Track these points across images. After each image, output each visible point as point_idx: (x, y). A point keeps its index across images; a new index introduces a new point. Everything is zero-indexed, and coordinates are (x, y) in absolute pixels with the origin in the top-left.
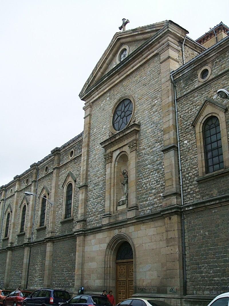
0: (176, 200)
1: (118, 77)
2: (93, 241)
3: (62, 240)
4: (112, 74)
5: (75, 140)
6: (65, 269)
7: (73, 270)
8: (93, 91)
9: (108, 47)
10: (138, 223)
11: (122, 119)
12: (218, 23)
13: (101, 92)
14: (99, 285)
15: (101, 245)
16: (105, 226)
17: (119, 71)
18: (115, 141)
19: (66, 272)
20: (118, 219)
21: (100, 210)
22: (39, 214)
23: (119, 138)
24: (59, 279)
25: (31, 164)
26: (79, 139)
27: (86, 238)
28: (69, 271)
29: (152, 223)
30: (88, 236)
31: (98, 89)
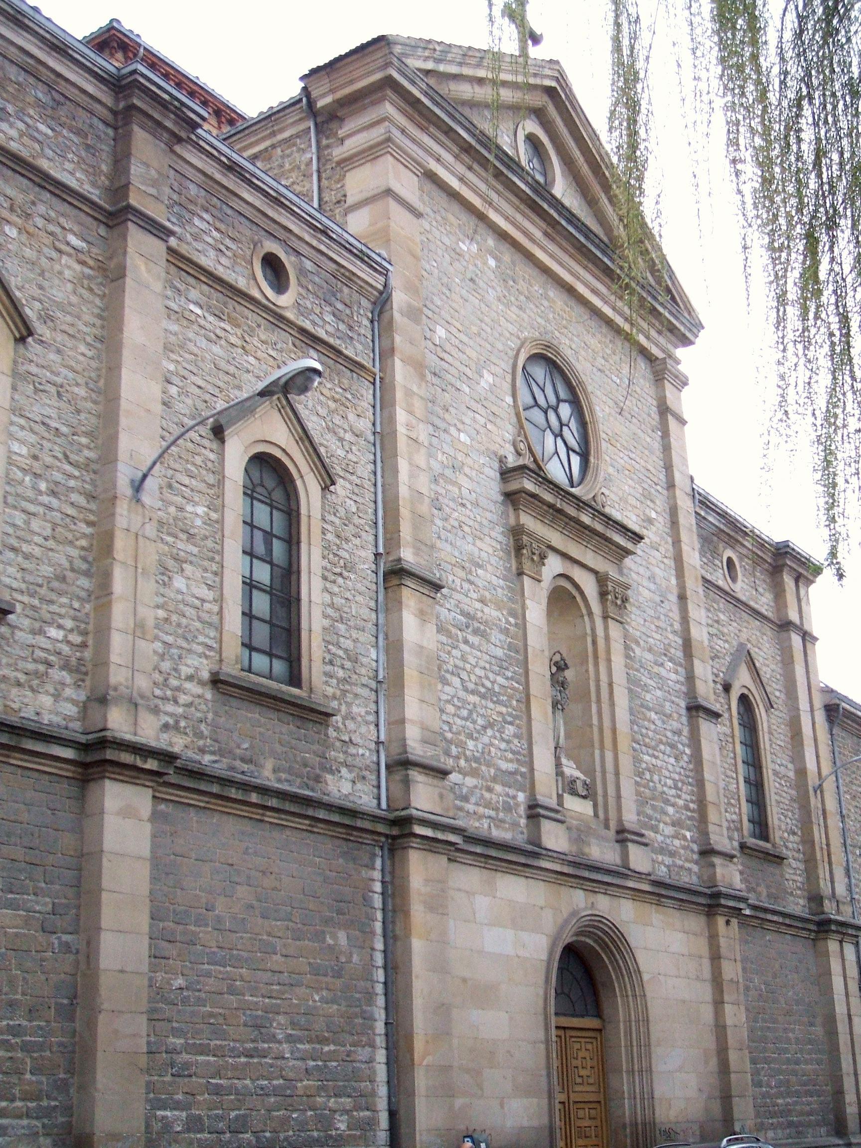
0: (715, 873)
1: (538, 234)
2: (482, 903)
3: (245, 811)
4: (545, 206)
5: (331, 238)
6: (281, 1019)
7: (349, 1038)
8: (449, 132)
9: (571, 90)
10: (213, 801)
11: (559, 440)
12: (104, 22)
13: (480, 196)
14: (525, 1123)
15: (525, 936)
16: (552, 859)
17: (558, 233)
18: (571, 518)
19: (290, 1039)
20: (586, 850)
21: (504, 766)
22: (317, 584)
23: (587, 527)
24: (230, 1090)
25: (128, 24)
26: (354, 265)
27: (397, 859)
28: (324, 1041)
29: (677, 914)
30: (456, 864)
31: (464, 157)
